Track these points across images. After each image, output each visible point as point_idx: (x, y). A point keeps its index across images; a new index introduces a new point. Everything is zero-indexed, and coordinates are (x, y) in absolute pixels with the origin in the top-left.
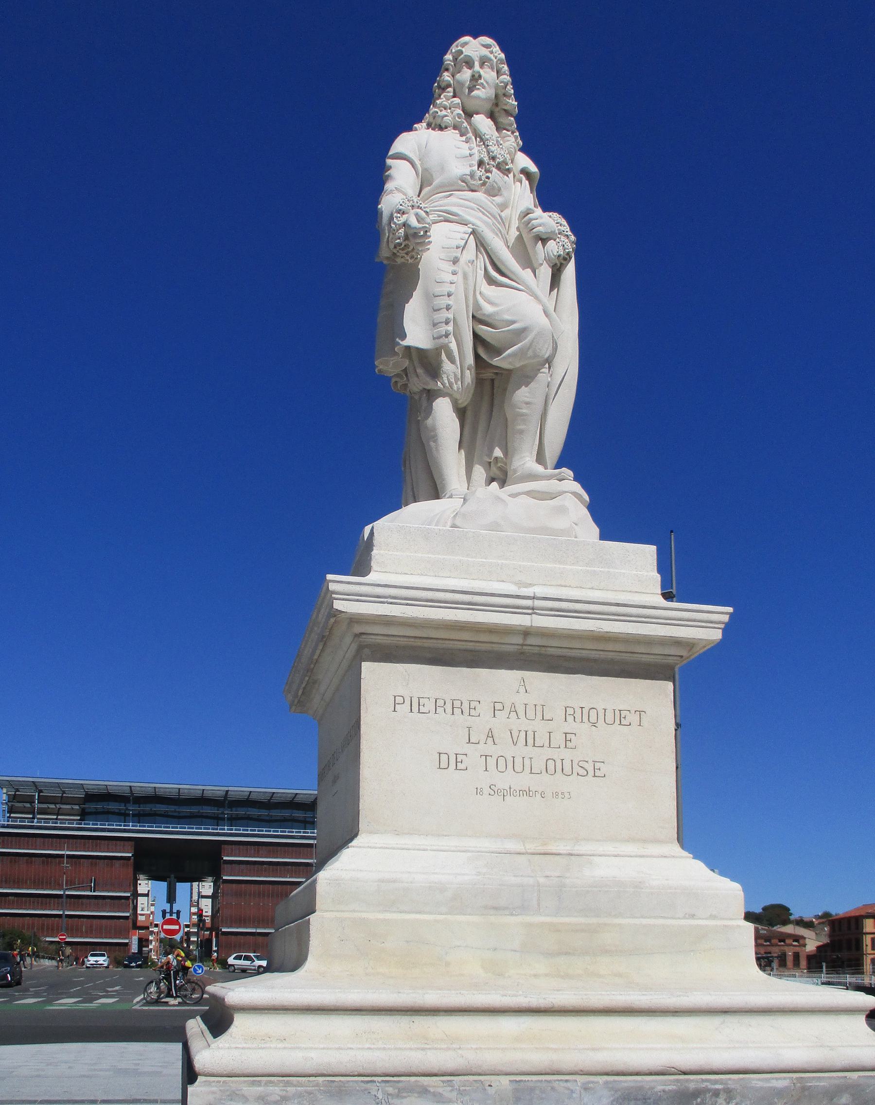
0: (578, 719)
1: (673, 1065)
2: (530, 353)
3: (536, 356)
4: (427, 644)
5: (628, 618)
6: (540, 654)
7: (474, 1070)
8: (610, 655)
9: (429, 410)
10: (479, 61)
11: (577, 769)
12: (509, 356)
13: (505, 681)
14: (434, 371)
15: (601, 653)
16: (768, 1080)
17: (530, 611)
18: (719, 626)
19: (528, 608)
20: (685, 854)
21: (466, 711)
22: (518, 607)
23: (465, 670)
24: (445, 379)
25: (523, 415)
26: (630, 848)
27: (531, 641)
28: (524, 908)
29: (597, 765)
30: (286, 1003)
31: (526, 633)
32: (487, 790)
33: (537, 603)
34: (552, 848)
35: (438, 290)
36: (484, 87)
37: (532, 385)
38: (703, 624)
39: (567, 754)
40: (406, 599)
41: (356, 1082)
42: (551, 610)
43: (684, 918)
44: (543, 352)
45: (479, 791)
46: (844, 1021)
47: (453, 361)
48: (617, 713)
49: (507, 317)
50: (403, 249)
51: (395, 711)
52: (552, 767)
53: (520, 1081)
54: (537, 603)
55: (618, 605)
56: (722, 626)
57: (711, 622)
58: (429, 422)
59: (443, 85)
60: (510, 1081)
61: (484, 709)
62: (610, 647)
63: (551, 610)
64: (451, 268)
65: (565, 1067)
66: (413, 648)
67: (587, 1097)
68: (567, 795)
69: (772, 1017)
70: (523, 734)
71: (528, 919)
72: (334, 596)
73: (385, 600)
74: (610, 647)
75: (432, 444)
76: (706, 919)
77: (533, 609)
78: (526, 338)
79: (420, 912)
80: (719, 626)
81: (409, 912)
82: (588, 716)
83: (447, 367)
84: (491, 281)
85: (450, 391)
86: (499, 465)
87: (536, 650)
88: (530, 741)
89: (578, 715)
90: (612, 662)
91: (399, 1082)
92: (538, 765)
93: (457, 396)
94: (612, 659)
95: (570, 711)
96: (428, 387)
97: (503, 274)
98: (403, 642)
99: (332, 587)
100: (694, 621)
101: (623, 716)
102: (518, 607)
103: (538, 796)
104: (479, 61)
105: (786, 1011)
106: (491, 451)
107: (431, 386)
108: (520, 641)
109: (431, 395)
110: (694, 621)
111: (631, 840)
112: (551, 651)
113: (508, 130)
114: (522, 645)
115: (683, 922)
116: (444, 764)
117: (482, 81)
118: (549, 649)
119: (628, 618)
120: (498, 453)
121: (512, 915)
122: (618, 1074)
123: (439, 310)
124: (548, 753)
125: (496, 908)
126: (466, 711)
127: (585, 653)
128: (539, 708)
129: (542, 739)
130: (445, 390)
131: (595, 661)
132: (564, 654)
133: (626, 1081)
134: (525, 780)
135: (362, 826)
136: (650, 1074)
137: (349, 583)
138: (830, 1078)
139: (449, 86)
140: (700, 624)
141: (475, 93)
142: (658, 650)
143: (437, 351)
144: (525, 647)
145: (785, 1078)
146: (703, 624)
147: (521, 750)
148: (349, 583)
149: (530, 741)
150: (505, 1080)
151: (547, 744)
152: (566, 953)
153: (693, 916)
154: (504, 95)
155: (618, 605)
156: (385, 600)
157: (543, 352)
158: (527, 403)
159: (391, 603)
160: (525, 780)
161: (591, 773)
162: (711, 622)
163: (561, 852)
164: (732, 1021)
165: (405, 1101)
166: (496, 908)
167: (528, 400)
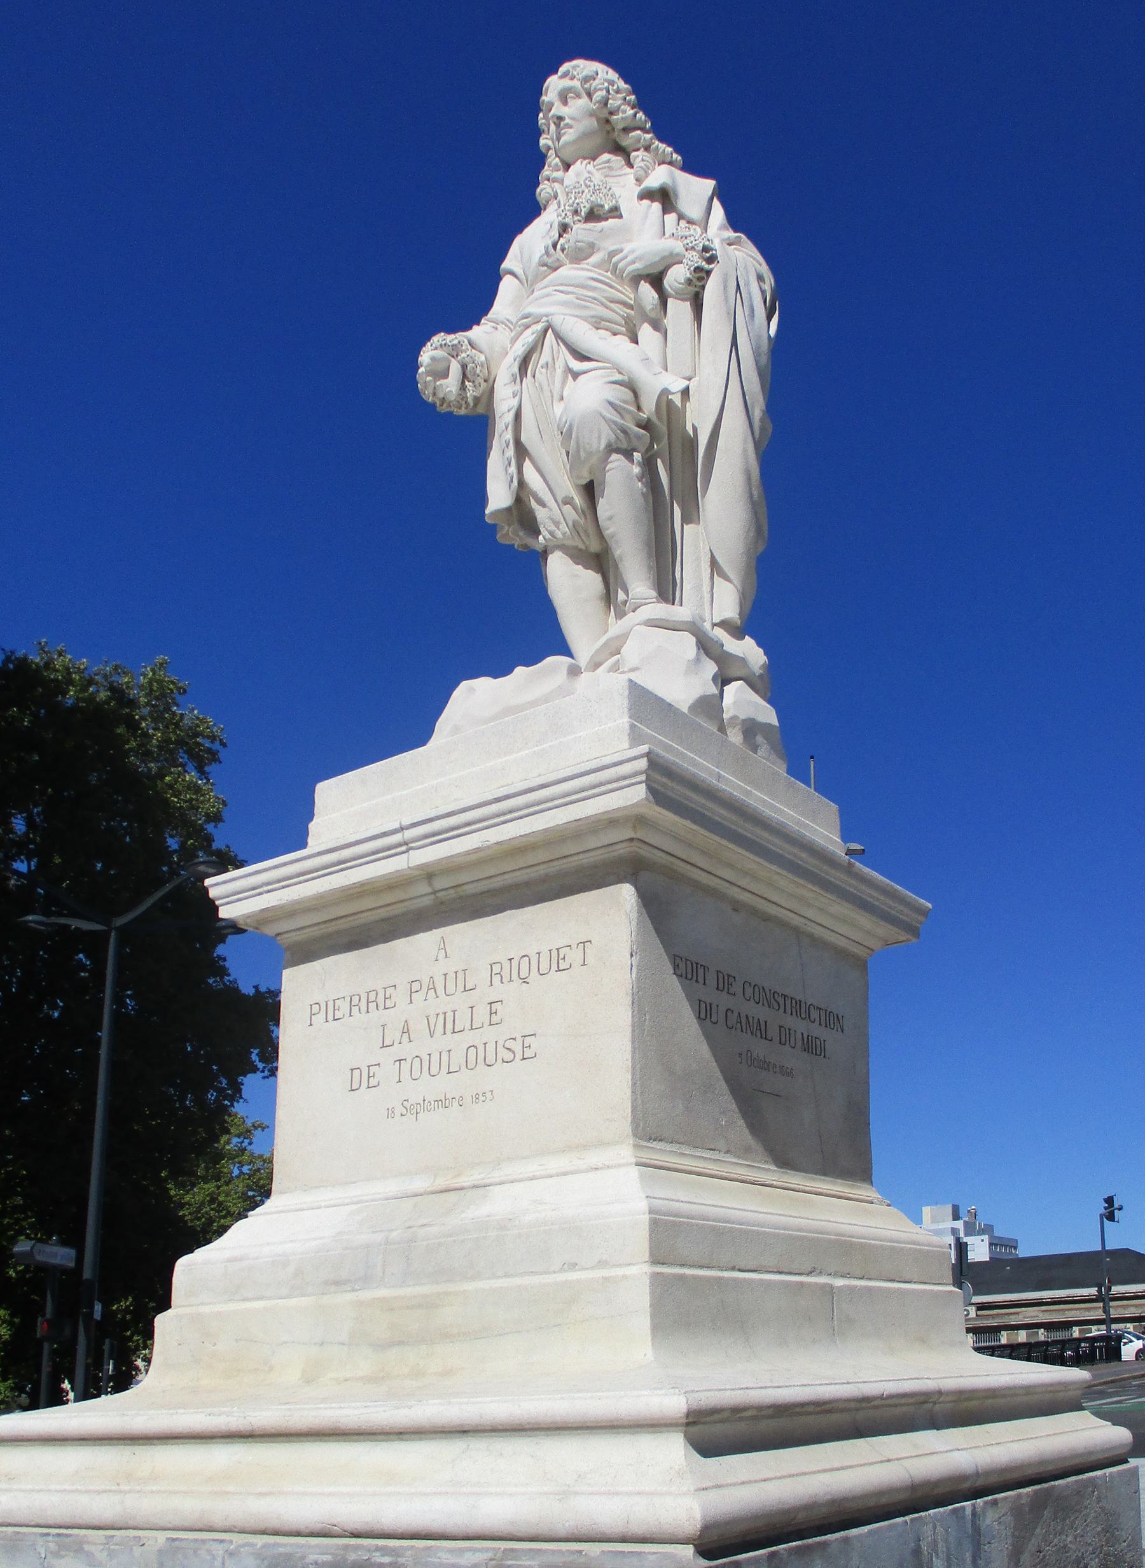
0: (506, 979)
1: (332, 1521)
3: (590, 454)
4: (342, 925)
5: (517, 814)
6: (461, 898)
7: (131, 1523)
8: (542, 870)
10: (579, 92)
13: (420, 949)
15: (528, 870)
16: (462, 1551)
17: (404, 848)
18: (638, 779)
19: (400, 845)
21: (381, 1006)
22: (389, 848)
26: (561, 1163)
27: (439, 884)
28: (366, 1280)
29: (528, 1040)
30: (22, 1433)
31: (429, 873)
32: (399, 1109)
33: (409, 834)
34: (464, 1181)
36: (571, 127)
38: (615, 785)
39: (490, 1035)
40: (279, 881)
41: (35, 1534)
42: (426, 837)
43: (562, 1270)
44: (595, 446)
45: (390, 1113)
46: (646, 1443)
48: (554, 953)
52: (479, 1058)
53: (176, 1539)
54: (409, 834)
55: (498, 800)
56: (643, 777)
57: (625, 778)
60: (168, 1539)
61: (400, 996)
62: (531, 859)
63: (426, 837)
65: (218, 1520)
66: (329, 936)
67: (231, 1566)
68: (489, 1095)
69: (535, 1440)
70: (441, 1017)
71: (366, 1295)
74: (531, 859)
76: (592, 1268)
77: (406, 844)
79: (261, 1298)
80: (638, 779)
82: (517, 969)
85: (559, 543)
88: (449, 1026)
89: (506, 973)
90: (545, 879)
91: (67, 1536)
92: (458, 1058)
93: (569, 543)
94: (547, 875)
95: (496, 968)
97: (589, 359)
98: (316, 932)
99: (213, 893)
100: (601, 784)
101: (561, 956)
102: (389, 848)
103: (455, 1104)
104: (579, 92)
105: (142, 1438)
108: (429, 890)
110: (601, 784)
111: (568, 1149)
112: (470, 889)
113: (638, 150)
115: (562, 1277)
117: (567, 121)
118: (464, 887)
119: (517, 814)
122: (356, 1535)
124: (469, 1038)
125: (337, 1283)
126: (381, 1006)
127: (509, 879)
128: (460, 976)
129: (463, 1022)
131: (527, 884)
132: (485, 889)
133: (285, 1545)
134: (443, 1085)
135: (275, 1187)
136: (312, 1534)
137: (225, 882)
138: (554, 1552)
140: (610, 787)
141: (563, 140)
142: (592, 842)
144: (439, 894)
145: (487, 1550)
146: (615, 785)
147: (442, 1042)
148: (225, 882)
149: (449, 1026)
150: (162, 1536)
151: (468, 1026)
152: (401, 1343)
153: (573, 1266)
154: (611, 113)
155: (498, 800)
157: (595, 446)
160: (443, 1085)
161: (519, 1056)
162: (625, 778)
163: (465, 1184)
164: (478, 1446)
165: (63, 1562)
166: (337, 1283)
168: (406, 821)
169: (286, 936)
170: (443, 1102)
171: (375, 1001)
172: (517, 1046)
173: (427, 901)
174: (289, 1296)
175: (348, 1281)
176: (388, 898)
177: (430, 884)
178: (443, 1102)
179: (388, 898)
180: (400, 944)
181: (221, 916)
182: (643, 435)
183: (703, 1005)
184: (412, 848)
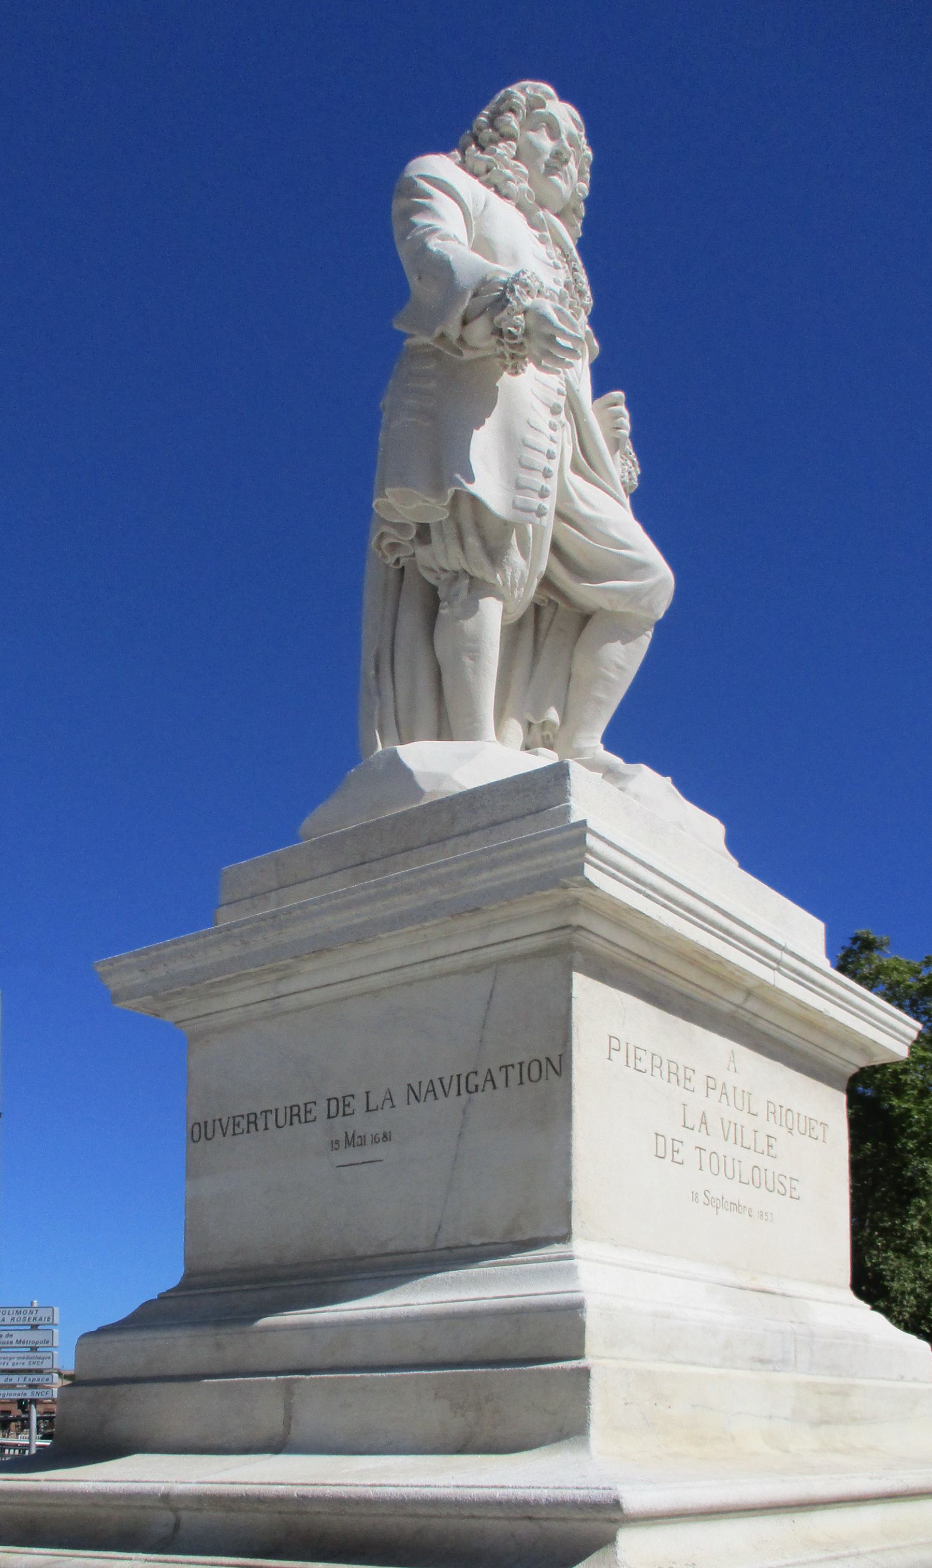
2: (644, 602)
4: (649, 970)
6: (748, 1024)
9: (471, 609)
11: (778, 1186)
12: (614, 590)
13: (716, 1050)
14: (495, 555)
17: (775, 965)
20: (862, 1303)
23: (681, 1022)
24: (509, 573)
25: (608, 679)
35: (531, 437)
37: (631, 645)
47: (524, 555)
49: (614, 533)
50: (512, 346)
51: (609, 1059)
58: (469, 625)
59: (504, 130)
64: (549, 418)
72: (588, 856)
73: (643, 889)
75: (468, 661)
78: (642, 579)
79: (693, 1364)
81: (684, 1363)
83: (515, 557)
84: (576, 468)
86: (545, 733)
87: (747, 1017)
96: (477, 573)
106: (539, 710)
107: (482, 571)
109: (479, 588)
112: (761, 1025)
114: (739, 1006)
116: (196, 1137)
120: (553, 715)
121: (775, 1370)
123: (533, 469)
125: (761, 1361)
130: (503, 591)
139: (512, 137)
143: (506, 527)
144: (740, 1011)
151: (752, 1147)
153: (902, 1378)
156: (643, 889)
158: (619, 667)
159: (648, 896)
166: (761, 1361)
167: (621, 662)
168: (791, 947)
169: (592, 937)
170: (736, 1207)
171: (679, 1076)
172: (787, 1183)
173: (726, 1007)
174: (721, 1367)
175: (769, 1362)
176: (709, 983)
177: (746, 1000)
178: (736, 1207)
179: (709, 983)
180: (698, 1030)
181: (912, 1027)
182: (637, 568)
183: (661, 1139)
184: (778, 970)
